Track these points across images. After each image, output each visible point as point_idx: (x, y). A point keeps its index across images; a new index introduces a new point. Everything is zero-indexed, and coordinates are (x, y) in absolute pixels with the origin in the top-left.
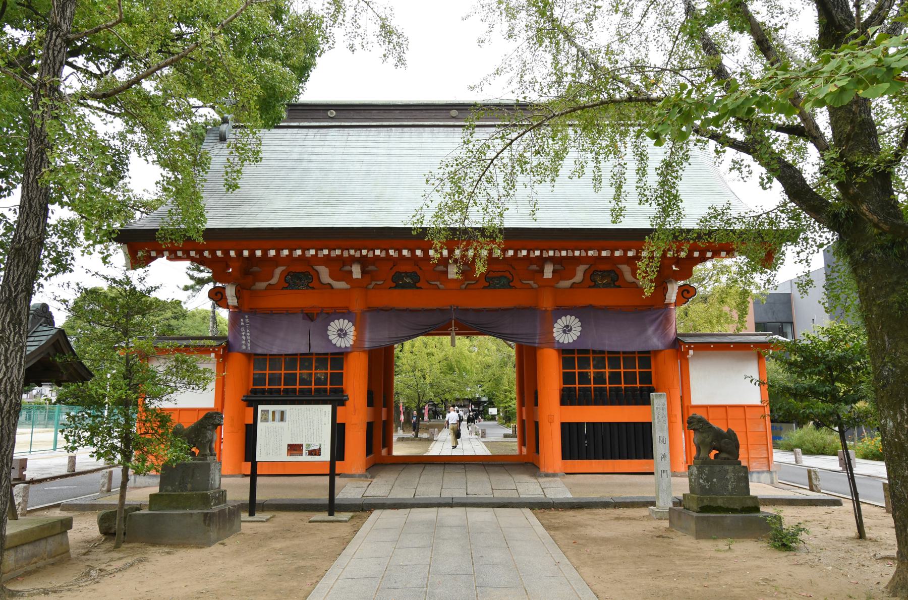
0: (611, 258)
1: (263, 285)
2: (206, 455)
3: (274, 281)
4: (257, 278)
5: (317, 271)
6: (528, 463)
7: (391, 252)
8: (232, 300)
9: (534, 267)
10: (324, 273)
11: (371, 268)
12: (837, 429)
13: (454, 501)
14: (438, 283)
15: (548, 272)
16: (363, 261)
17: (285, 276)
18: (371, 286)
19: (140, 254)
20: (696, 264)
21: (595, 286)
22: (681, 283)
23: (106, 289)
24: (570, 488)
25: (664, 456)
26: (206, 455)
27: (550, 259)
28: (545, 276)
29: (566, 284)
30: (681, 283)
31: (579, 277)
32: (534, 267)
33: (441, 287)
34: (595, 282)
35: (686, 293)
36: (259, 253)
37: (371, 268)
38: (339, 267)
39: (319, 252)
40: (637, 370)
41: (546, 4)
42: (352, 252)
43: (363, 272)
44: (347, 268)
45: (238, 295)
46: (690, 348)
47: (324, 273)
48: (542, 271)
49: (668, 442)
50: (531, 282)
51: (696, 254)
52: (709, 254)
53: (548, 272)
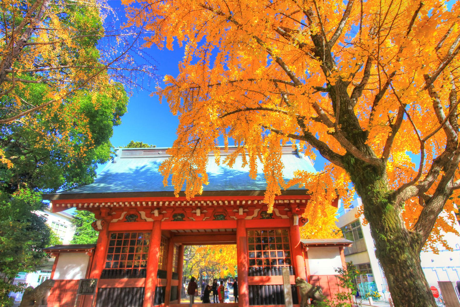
1: (115, 220)
3: (121, 218)
4: (114, 217)
5: (140, 214)
8: (100, 227)
11: (205, 211)
12: (185, 246)
15: (241, 211)
17: (125, 217)
18: (163, 220)
21: (263, 218)
22: (300, 216)
24: (288, 293)
29: (249, 218)
30: (300, 216)
31: (255, 214)
32: (235, 210)
33: (194, 220)
34: (262, 216)
35: (303, 221)
37: (205, 211)
38: (149, 210)
41: (2, 168)
43: (160, 213)
44: (194, 211)
45: (102, 224)
50: (234, 217)
53: (241, 211)
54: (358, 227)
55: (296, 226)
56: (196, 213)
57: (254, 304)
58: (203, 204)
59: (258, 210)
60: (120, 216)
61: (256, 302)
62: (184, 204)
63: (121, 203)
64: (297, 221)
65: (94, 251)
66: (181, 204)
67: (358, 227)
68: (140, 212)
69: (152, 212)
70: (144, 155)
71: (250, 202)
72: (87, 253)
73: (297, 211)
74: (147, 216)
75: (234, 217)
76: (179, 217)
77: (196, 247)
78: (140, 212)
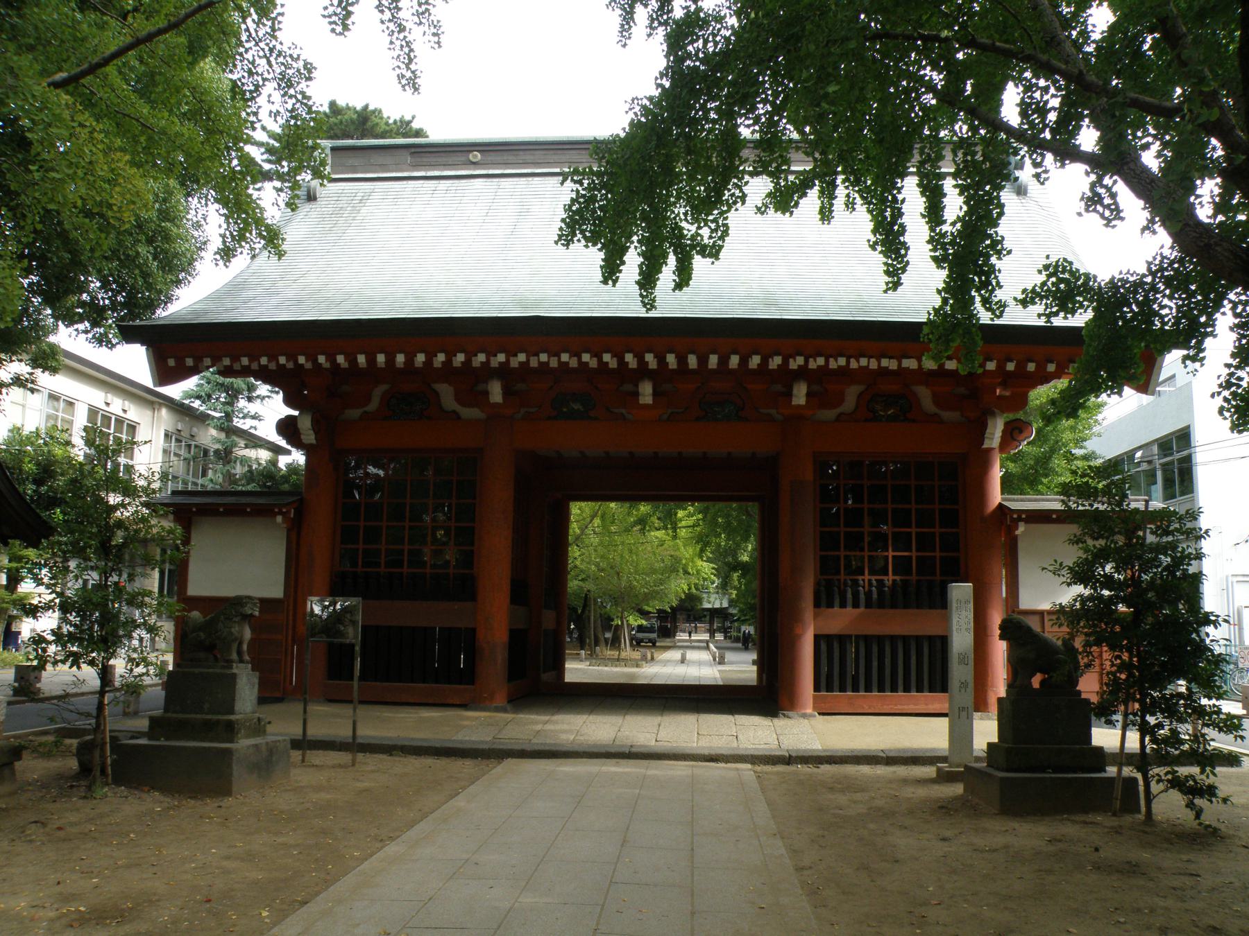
0: (902, 372)
1: (354, 413)
2: (232, 661)
3: (374, 405)
5: (437, 394)
6: (767, 697)
7: (586, 357)
8: (309, 437)
9: (778, 387)
10: (447, 394)
13: (633, 750)
14: (623, 411)
15: (800, 394)
16: (503, 372)
19: (171, 362)
20: (1034, 386)
22: (1011, 416)
23: (718, 675)
25: (964, 685)
26: (232, 661)
27: (802, 373)
28: (795, 402)
29: (829, 414)
30: (1011, 416)
31: (850, 403)
32: (778, 387)
36: (692, 361)
39: (512, 359)
40: (938, 554)
42: (544, 357)
43: (507, 392)
44: (628, 387)
46: (1020, 519)
47: (447, 394)
48: (789, 394)
49: (972, 663)
50: (773, 412)
51: (1031, 367)
52: (1051, 368)
53: (800, 394)
54: (1185, 453)
55: (990, 450)
56: (636, 394)
57: (830, 605)
58: (567, 363)
59: (860, 388)
60: (368, 399)
61: (837, 602)
62: (520, 363)
63: (302, 360)
64: (998, 434)
65: (299, 512)
66: (508, 361)
67: (1185, 453)
68: (437, 386)
69: (481, 387)
70: (416, 167)
71: (776, 361)
72: (279, 519)
73: (1000, 397)
74: (458, 400)
75: (773, 412)
76: (577, 406)
77: (574, 552)
78: (437, 386)
